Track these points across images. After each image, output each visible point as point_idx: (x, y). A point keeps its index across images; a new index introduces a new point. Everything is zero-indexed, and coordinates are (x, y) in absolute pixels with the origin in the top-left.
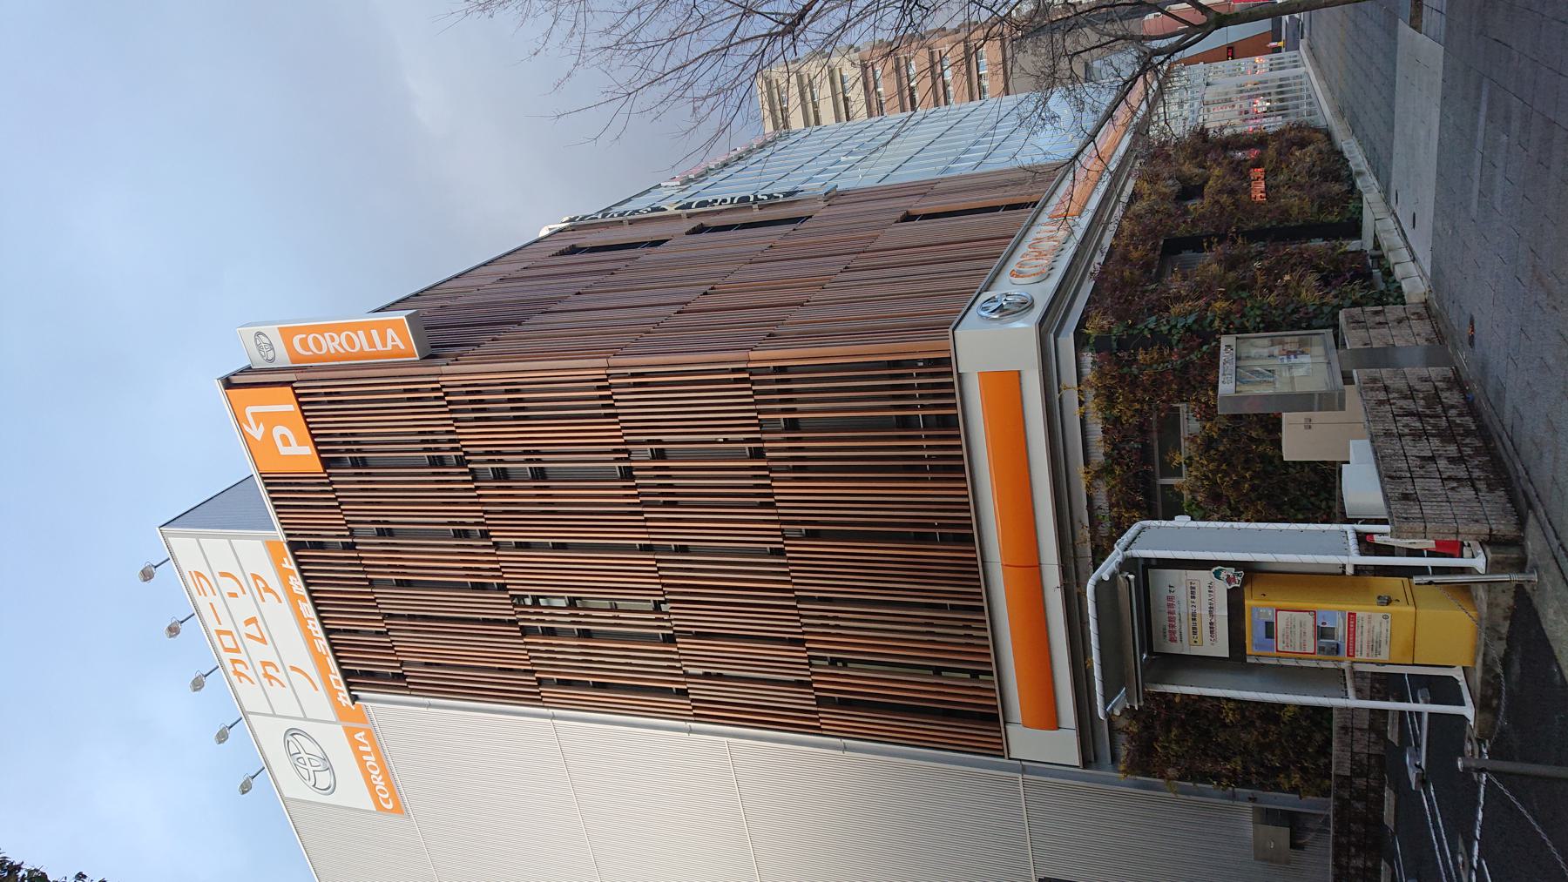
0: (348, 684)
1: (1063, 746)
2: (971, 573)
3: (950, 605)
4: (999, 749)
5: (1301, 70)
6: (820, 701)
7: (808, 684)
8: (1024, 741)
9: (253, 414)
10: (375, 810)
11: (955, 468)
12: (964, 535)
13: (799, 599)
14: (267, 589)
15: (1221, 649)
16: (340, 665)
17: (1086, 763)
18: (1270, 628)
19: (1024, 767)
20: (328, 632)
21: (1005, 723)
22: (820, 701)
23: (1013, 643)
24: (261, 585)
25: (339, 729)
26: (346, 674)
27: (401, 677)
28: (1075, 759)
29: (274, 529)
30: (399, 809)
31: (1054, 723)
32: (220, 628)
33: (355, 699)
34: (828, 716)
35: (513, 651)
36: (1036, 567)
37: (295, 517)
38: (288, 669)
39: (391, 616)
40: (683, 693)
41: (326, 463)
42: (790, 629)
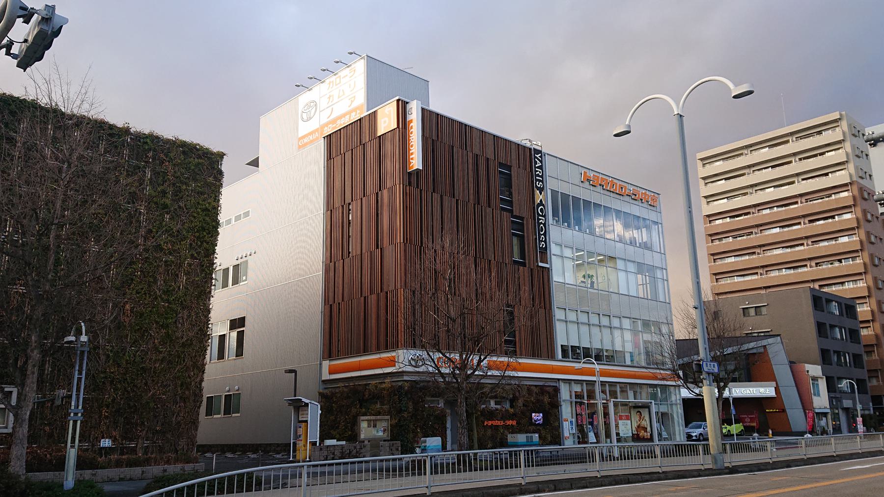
0: (328, 136)
1: (326, 376)
2: (358, 353)
3: (71, 443)
4: (324, 359)
5: (771, 436)
6: (331, 305)
7: (334, 302)
8: (326, 364)
9: (391, 110)
10: (299, 137)
11: (378, 350)
12: (366, 351)
13: (352, 300)
14: (352, 101)
15: (300, 419)
16: (332, 133)
17: (323, 381)
18: (300, 427)
19: (321, 364)
20: (340, 130)
21: (330, 360)
22: (331, 305)
23: (347, 362)
24: (353, 99)
25: (317, 126)
26: (330, 135)
27: (330, 159)
28: (323, 379)
29: (367, 111)
30: (300, 147)
31: (330, 373)
32: (341, 77)
33: (324, 138)
34: (328, 307)
35: (338, 204)
36: (360, 369)
37: (367, 119)
38: (332, 107)
39: (345, 155)
40: (331, 262)
41: (380, 137)
42: (345, 299)
